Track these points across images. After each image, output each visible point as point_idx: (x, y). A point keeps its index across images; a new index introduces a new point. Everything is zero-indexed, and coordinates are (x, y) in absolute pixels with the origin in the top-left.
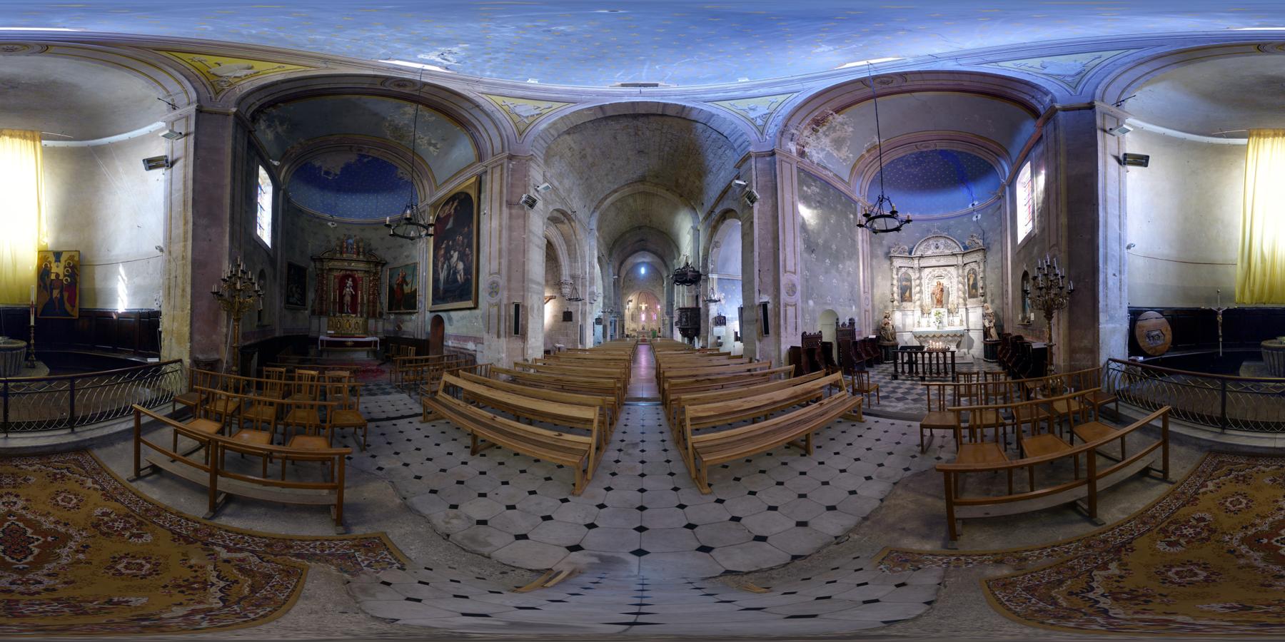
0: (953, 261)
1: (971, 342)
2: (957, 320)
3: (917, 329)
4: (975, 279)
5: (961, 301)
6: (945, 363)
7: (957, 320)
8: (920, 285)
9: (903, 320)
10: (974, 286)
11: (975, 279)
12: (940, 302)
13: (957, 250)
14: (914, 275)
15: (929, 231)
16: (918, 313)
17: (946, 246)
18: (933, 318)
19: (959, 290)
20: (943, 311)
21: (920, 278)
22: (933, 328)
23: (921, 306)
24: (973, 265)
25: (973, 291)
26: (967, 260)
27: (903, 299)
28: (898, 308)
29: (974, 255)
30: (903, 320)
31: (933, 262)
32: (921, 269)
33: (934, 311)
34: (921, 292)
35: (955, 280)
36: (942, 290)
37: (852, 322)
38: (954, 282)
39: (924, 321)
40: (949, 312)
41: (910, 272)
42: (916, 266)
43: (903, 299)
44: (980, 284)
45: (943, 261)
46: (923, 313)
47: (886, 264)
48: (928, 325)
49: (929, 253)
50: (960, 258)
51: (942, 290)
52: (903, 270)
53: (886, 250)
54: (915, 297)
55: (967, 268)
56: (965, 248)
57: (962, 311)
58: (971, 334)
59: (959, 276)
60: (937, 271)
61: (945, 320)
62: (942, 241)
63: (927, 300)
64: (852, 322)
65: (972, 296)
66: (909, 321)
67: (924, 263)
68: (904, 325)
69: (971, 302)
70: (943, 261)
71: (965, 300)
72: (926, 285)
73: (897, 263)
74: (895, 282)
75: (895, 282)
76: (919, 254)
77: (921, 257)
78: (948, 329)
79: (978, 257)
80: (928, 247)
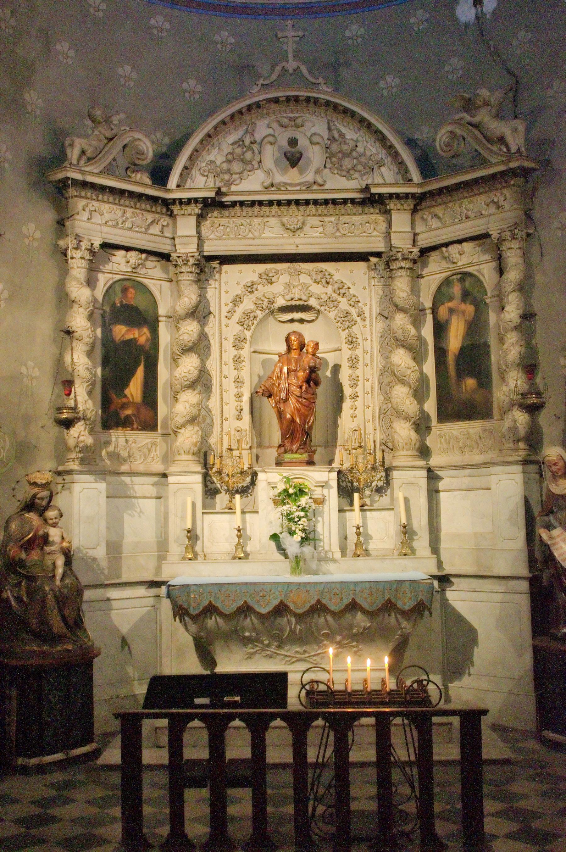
0: (363, 231)
1: (460, 642)
2: (382, 527)
3: (183, 573)
4: (476, 326)
5: (404, 431)
6: (425, 760)
7: (382, 527)
8: (200, 346)
9: (115, 523)
10: (474, 360)
11: (476, 326)
12: (301, 437)
13: (385, 180)
14: (169, 296)
15: (244, 70)
16: (187, 483)
17: (337, 156)
18: (266, 518)
19: (390, 376)
20: (320, 479)
21: (200, 313)
22: (266, 570)
23: (204, 456)
24: (469, 258)
25: (460, 386)
26: (432, 229)
27: (112, 417)
28: (90, 459)
29: (478, 202)
30: (115, 523)
31: (269, 234)
32: (208, 264)
33: (271, 480)
34: (201, 382)
35: (370, 330)
36: (312, 379)
37: (117, 715)
38: (367, 344)
39: (219, 529)
40: (346, 491)
41: (153, 276)
42: (187, 248)
43: (112, 417)
44: (506, 351)
45: (316, 234)
46: (210, 492)
47: (34, 224)
48: (236, 547)
49: (251, 185)
50: (401, 220)
51: (312, 379)
52: (120, 263)
53: (36, 142)
54: (175, 407)
55: (435, 271)
56: (427, 168)
57: (409, 483)
58: (456, 597)
59: (390, 307)
60: (286, 284)
61: (328, 525)
62: (316, 125)
63: (231, 418)
64: (117, 715)
65: (454, 409)
66: (140, 525)
67: (224, 234)
68: (115, 549)
69: (451, 439)
70: (316, 234)
71: (422, 426)
72: (226, 352)
73: (96, 220)
74: (79, 321)
75: (79, 321)
76: (201, 186)
77: (213, 204)
78: (343, 571)
79: (491, 213)
80: (245, 157)
